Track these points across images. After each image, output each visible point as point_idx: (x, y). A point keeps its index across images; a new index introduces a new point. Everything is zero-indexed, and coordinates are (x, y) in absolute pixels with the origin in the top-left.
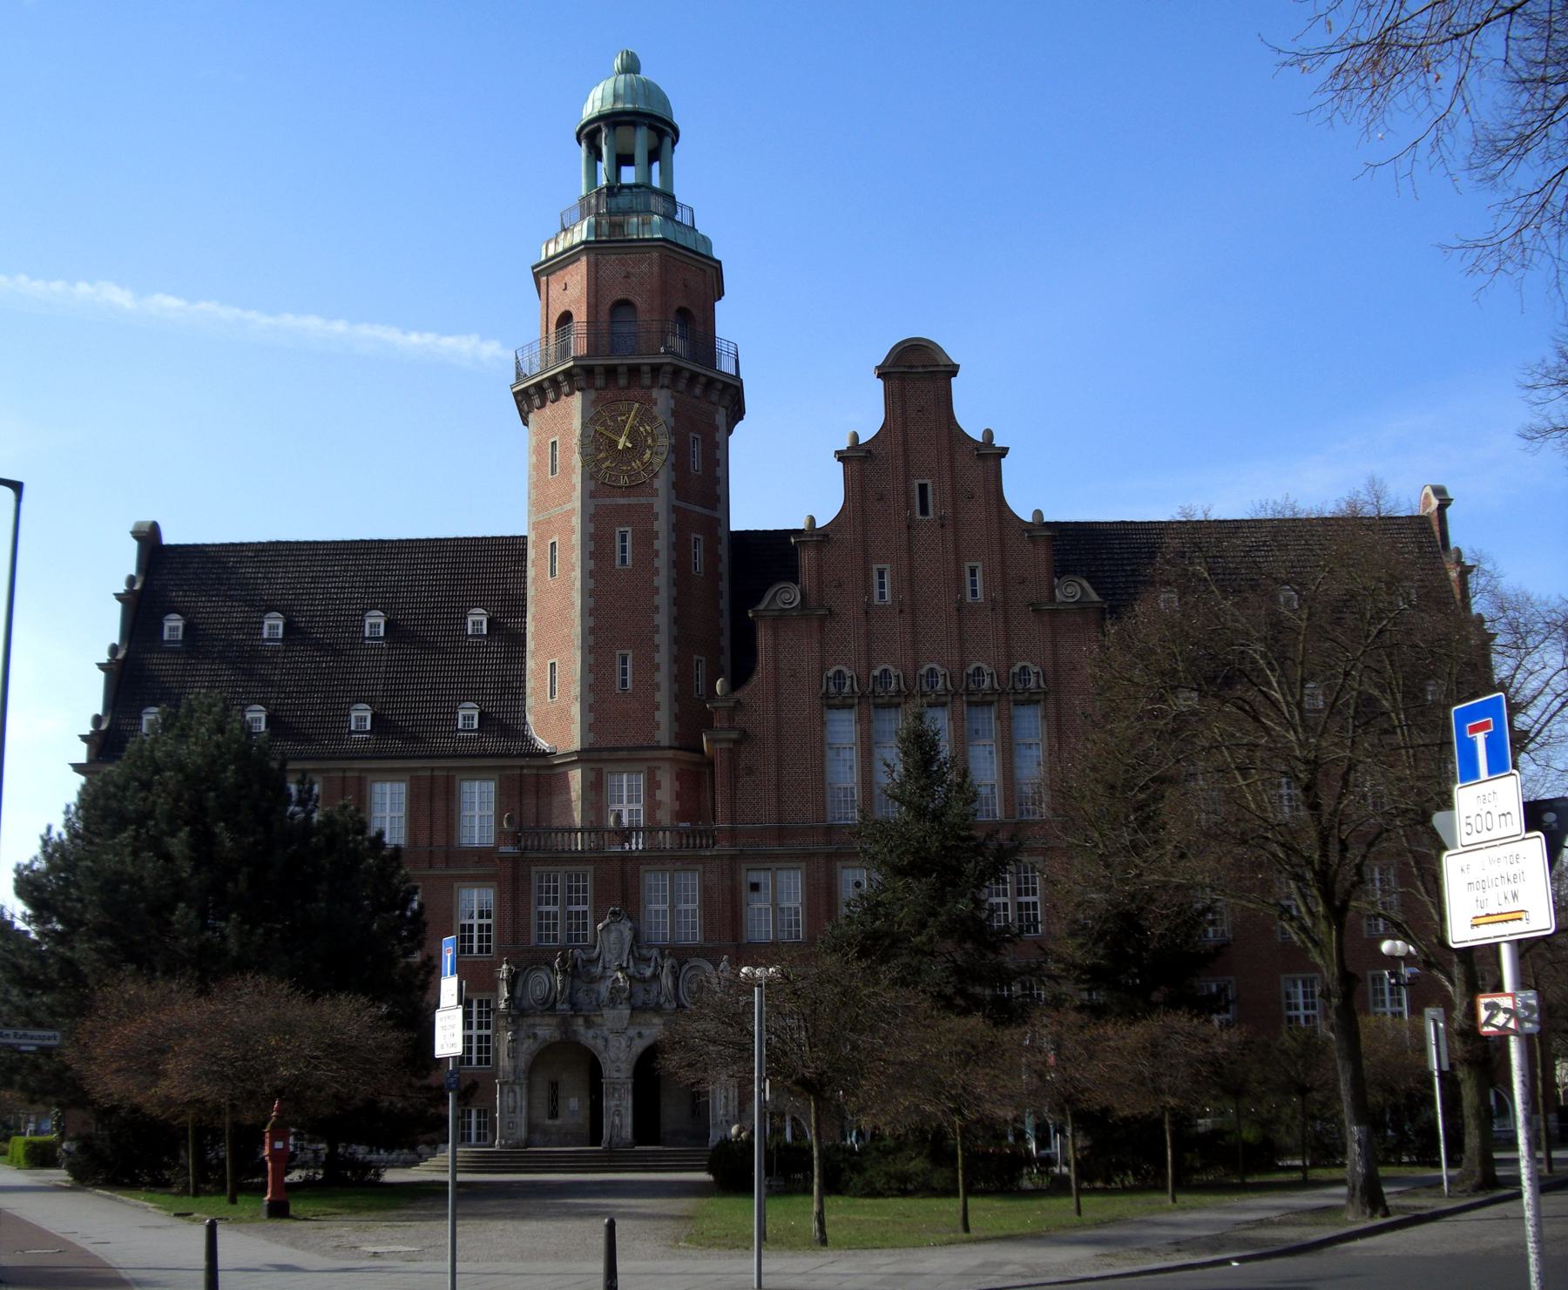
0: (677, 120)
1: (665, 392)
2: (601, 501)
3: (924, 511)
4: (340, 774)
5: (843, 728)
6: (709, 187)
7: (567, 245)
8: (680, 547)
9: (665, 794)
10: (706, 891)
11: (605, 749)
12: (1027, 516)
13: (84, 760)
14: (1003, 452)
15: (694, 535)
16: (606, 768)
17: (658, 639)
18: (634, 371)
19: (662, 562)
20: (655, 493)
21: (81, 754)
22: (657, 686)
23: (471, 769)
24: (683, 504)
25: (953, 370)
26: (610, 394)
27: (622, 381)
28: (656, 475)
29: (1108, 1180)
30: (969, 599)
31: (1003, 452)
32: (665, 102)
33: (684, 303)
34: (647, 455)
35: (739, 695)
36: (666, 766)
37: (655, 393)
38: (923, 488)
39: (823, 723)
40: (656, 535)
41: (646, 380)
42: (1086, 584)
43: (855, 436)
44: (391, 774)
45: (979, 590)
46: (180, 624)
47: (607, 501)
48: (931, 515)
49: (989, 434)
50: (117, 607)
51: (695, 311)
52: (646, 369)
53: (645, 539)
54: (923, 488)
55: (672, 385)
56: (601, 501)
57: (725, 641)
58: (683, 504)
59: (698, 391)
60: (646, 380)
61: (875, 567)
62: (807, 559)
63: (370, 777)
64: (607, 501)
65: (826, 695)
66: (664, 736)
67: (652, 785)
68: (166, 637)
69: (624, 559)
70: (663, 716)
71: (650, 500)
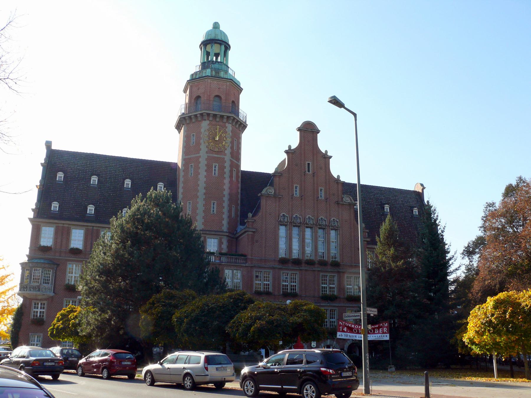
0: (230, 43)
1: (230, 125)
2: (209, 155)
3: (309, 171)
4: (62, 225)
5: (282, 231)
6: (237, 65)
7: (200, 76)
8: (231, 171)
9: (225, 246)
10: (243, 276)
11: (207, 231)
12: (335, 174)
13: (32, 217)
14: (331, 157)
15: (214, 164)
16: (207, 236)
17: (224, 199)
18: (222, 117)
19: (227, 175)
20: (225, 155)
21: (31, 215)
22: (223, 213)
23: (77, 225)
24: (232, 159)
25: (318, 132)
26: (214, 123)
27: (218, 120)
28: (226, 149)
29: (494, 333)
30: (320, 198)
31: (331, 157)
32: (225, 35)
33: (234, 100)
34: (224, 143)
35: (255, 218)
36: (225, 237)
37: (227, 125)
38: (309, 164)
39: (279, 229)
40: (225, 167)
41: (225, 120)
42: (351, 198)
43: (290, 147)
44: (49, 224)
45: (322, 195)
46: (63, 176)
47: (211, 155)
48: (311, 173)
49: (326, 151)
50: (41, 168)
51: (223, 97)
52: (226, 117)
53: (222, 168)
54: (309, 164)
55: (232, 123)
56: (209, 155)
57: (239, 202)
58: (232, 159)
59: (237, 126)
60: (225, 120)
61: (295, 185)
62: (276, 180)
63: (72, 227)
64: (211, 155)
65: (280, 221)
66: (225, 228)
67: (220, 243)
68: (57, 179)
69: (215, 173)
70: (225, 222)
71: (224, 156)
